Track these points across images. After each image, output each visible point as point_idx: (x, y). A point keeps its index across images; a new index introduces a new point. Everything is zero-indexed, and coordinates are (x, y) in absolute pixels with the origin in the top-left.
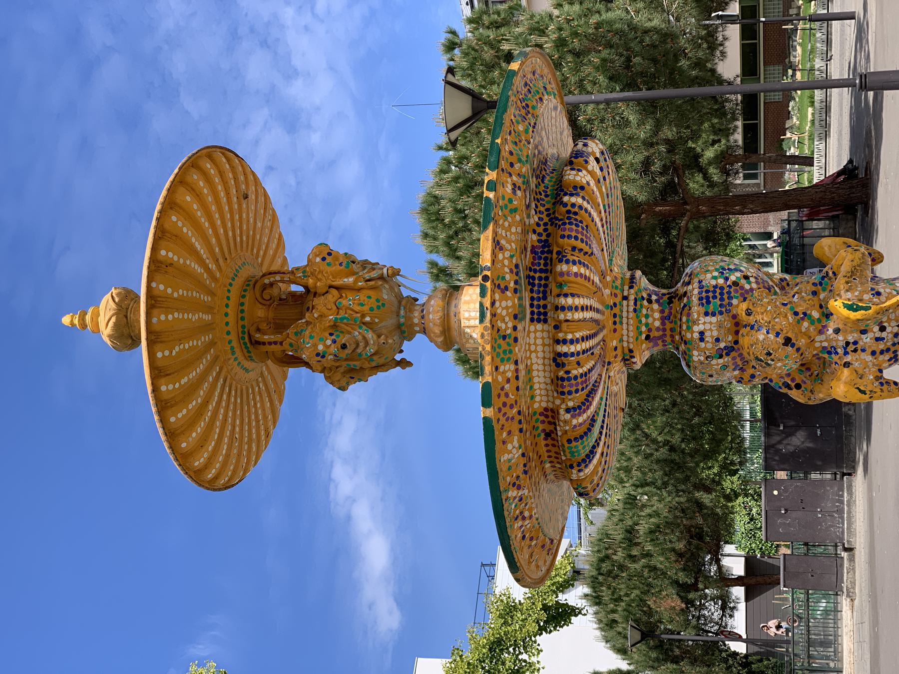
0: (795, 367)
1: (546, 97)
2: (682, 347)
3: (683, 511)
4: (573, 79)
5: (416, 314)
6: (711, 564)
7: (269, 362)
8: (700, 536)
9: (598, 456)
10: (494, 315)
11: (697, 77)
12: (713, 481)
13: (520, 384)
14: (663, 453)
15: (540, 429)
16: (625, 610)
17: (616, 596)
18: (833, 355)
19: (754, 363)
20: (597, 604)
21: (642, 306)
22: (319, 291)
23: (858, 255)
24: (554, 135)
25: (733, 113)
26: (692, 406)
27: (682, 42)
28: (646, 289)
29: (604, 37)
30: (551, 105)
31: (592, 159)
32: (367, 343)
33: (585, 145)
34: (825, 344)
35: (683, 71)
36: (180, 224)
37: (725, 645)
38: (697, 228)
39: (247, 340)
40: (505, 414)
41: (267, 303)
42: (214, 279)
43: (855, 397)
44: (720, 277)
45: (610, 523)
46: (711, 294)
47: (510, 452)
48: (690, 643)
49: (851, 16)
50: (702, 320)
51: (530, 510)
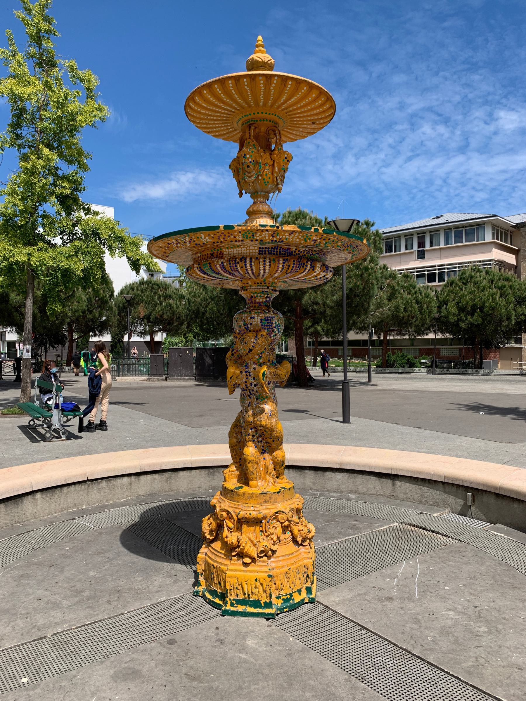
1: (351, 255)
2: (248, 310)
3: (179, 317)
4: (351, 274)
5: (262, 200)
7: (241, 133)
8: (169, 324)
9: (204, 276)
10: (262, 231)
12: (191, 329)
13: (233, 242)
14: (202, 310)
15: (215, 252)
19: (242, 337)
20: (140, 283)
22: (272, 156)
23: (284, 377)
24: (335, 259)
25: (334, 337)
27: (363, 317)
30: (347, 257)
31: (325, 274)
32: (250, 177)
33: (331, 271)
34: (249, 364)
36: (303, 91)
38: (290, 323)
39: (251, 122)
40: (221, 235)
41: (267, 133)
42: (278, 107)
43: (229, 376)
47: (205, 238)
50: (259, 318)
51: (181, 247)
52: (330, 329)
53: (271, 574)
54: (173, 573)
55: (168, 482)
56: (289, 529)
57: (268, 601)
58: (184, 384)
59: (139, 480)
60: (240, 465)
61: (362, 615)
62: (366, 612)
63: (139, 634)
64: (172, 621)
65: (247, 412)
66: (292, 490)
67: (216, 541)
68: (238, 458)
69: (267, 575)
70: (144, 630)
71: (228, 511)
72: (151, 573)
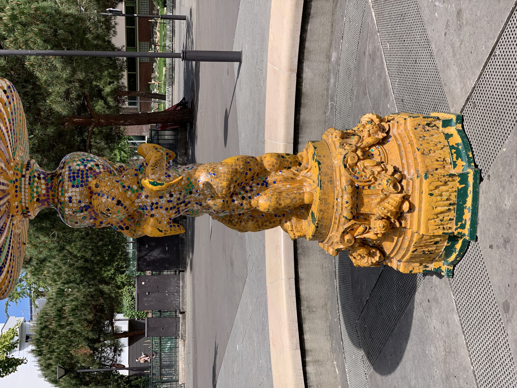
0: (123, 217)
2: (59, 206)
3: (92, 296)
4: (21, 40)
6: (108, 326)
8: (102, 311)
11: (97, 45)
12: (111, 278)
14: (80, 263)
16: (56, 357)
17: (51, 350)
18: (145, 210)
19: (100, 215)
20: (39, 355)
21: (34, 181)
23: (159, 154)
25: (121, 67)
26: (98, 236)
28: (37, 171)
29: (39, 16)
34: (141, 204)
35: (89, 41)
37: (116, 372)
44: (82, 165)
45: (48, 306)
46: (76, 175)
48: (96, 373)
49: (183, 18)
50: (71, 189)
52: (109, 73)
53: (423, 175)
54: (425, 304)
55: (314, 310)
56: (367, 149)
57: (458, 179)
58: (191, 288)
59: (311, 351)
60: (284, 215)
61: (477, 53)
62: (474, 48)
63: (497, 350)
64: (482, 305)
65: (209, 207)
66: (316, 145)
67: (382, 248)
68: (275, 219)
69: (424, 181)
70: (492, 344)
71: (343, 232)
72: (426, 334)
